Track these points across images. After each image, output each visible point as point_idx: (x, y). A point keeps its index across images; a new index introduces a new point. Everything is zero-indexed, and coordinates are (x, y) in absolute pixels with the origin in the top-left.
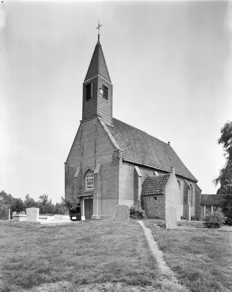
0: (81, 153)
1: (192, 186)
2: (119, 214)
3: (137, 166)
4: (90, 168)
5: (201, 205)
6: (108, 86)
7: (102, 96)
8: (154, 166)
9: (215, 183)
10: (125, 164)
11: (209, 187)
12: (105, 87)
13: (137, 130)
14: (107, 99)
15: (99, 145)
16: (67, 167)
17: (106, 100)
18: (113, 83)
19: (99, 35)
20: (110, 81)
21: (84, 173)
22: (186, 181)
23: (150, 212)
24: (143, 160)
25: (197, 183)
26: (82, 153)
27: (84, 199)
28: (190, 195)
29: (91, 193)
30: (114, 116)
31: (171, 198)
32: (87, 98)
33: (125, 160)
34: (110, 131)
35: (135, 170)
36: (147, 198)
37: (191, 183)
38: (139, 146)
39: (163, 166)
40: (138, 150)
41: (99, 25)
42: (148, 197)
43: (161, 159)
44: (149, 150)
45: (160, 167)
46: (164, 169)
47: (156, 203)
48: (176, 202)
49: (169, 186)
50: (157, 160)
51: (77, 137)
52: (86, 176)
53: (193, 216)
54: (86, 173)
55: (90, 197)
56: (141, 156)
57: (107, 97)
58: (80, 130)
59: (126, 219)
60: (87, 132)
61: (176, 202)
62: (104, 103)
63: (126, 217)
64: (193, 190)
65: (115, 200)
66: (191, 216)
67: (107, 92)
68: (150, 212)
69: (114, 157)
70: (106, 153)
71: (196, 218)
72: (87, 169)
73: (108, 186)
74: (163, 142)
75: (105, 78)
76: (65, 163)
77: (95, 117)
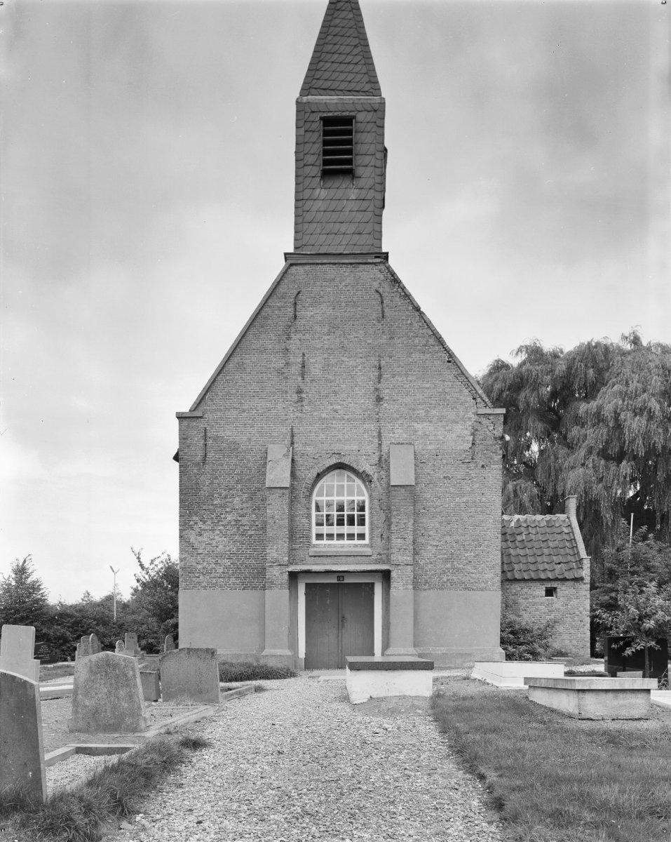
15: (400, 375)
16: (197, 440)
29: (352, 558)
32: (328, 160)
42: (523, 584)
47: (556, 606)
51: (266, 318)
55: (555, 585)
58: (288, 289)
69: (479, 437)
77: (378, 260)
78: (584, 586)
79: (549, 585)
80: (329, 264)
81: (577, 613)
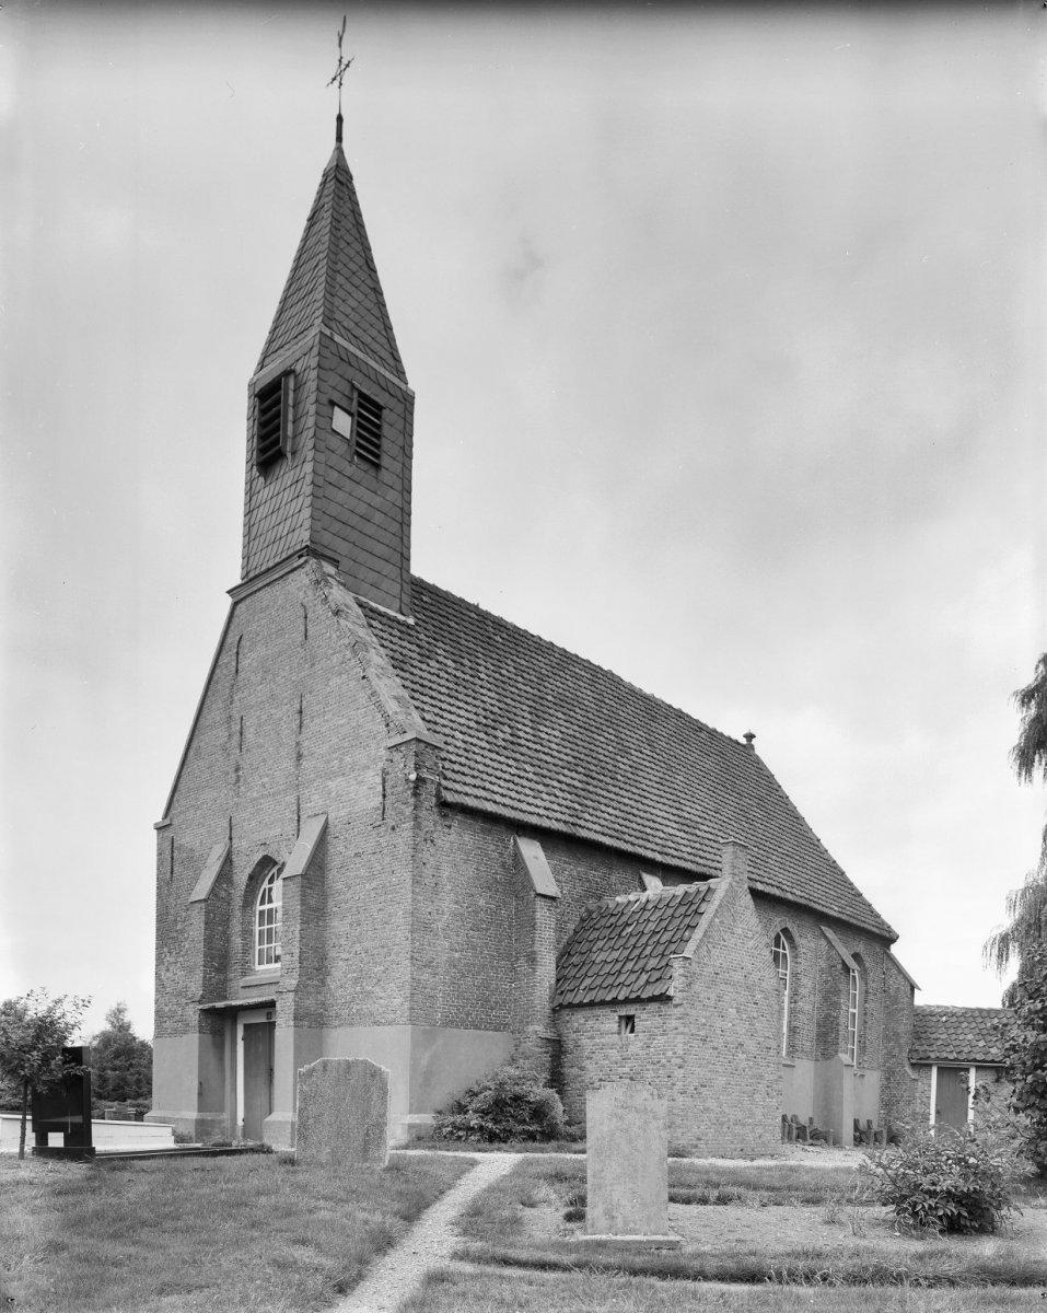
0: (231, 770)
1: (867, 965)
2: (317, 1118)
3: (534, 839)
4: (270, 852)
5: (913, 1065)
6: (381, 399)
7: (343, 448)
8: (641, 842)
9: (994, 958)
11: (957, 964)
12: (362, 395)
13: (567, 660)
14: (377, 467)
17: (372, 472)
18: (415, 382)
19: (340, 119)
20: (401, 373)
21: (241, 878)
22: (829, 933)
24: (577, 806)
26: (237, 770)
28: (856, 1011)
30: (419, 569)
31: (719, 1023)
32: (269, 458)
33: (449, 797)
34: (391, 653)
35: (517, 857)
36: (582, 1021)
37: (860, 947)
38: (561, 736)
39: (697, 845)
40: (555, 753)
41: (340, 61)
44: (625, 761)
45: (675, 853)
46: (701, 861)
48: (751, 1045)
49: (709, 951)
50: (666, 815)
51: (217, 682)
52: (255, 897)
53: (869, 1122)
54: (251, 878)
56: (564, 787)
57: (377, 456)
58: (232, 639)
59: (365, 1150)
60: (261, 651)
62: (360, 491)
63: (366, 1143)
64: (871, 984)
66: (856, 1122)
67: (379, 427)
70: (348, 759)
71: (885, 1135)
72: (257, 857)
73: (358, 947)
74: (713, 733)
75: (364, 346)
76: (159, 829)
77: (302, 560)
78: (675, 1011)
79: (624, 1011)
80: (265, 586)
81: (664, 1061)
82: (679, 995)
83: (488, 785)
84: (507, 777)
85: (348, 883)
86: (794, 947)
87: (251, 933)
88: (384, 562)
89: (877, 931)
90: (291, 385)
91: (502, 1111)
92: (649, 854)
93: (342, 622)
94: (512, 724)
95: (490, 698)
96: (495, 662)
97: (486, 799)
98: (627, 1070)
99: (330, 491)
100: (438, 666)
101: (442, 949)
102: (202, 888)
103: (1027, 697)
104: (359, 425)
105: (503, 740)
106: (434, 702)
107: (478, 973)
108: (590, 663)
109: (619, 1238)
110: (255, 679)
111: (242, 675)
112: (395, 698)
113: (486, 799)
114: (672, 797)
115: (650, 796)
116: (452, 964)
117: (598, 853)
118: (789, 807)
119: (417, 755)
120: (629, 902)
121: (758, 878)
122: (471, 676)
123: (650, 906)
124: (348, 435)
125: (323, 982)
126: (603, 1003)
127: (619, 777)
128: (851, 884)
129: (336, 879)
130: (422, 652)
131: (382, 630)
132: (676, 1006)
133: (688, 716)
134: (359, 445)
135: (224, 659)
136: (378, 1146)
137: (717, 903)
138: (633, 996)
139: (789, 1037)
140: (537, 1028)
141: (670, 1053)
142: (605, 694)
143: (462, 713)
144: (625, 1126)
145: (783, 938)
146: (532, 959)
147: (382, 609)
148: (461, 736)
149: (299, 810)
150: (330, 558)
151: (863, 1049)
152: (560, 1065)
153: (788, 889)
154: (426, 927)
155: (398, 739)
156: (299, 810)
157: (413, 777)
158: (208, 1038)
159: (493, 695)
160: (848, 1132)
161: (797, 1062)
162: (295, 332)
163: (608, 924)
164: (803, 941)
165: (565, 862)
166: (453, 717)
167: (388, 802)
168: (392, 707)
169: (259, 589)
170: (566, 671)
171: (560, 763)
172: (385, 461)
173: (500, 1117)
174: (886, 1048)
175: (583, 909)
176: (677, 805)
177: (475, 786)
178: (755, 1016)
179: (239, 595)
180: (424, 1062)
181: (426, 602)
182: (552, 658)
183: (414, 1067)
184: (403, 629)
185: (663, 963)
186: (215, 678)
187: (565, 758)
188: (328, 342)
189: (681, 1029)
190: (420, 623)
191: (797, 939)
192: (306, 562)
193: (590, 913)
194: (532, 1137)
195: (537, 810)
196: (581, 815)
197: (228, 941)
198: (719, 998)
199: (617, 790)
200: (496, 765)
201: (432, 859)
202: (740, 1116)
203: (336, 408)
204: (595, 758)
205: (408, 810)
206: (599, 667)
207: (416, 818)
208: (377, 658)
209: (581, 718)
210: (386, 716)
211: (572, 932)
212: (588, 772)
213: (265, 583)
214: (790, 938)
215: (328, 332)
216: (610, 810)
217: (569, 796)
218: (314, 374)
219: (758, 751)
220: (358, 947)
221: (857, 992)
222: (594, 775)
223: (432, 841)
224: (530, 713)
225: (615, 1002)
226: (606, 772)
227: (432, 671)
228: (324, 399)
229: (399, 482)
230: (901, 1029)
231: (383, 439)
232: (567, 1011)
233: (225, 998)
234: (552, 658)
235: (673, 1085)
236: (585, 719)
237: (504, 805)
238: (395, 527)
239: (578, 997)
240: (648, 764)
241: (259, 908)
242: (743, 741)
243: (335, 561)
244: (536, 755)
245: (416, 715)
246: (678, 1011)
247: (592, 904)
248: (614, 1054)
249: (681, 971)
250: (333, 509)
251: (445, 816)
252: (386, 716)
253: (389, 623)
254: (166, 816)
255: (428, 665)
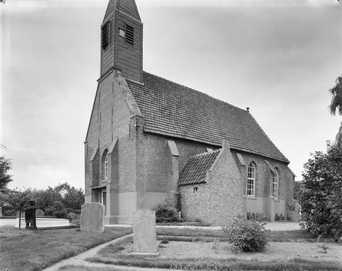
0: (99, 127)
1: (280, 170)
2: (86, 219)
8: (206, 139)
10: (149, 137)
12: (127, 25)
13: (191, 91)
14: (132, 44)
17: (131, 45)
20: (139, 19)
21: (101, 154)
22: (267, 162)
23: (190, 210)
24: (187, 131)
25: (288, 165)
26: (100, 127)
27: (103, 192)
28: (277, 183)
31: (221, 189)
33: (146, 130)
35: (167, 145)
36: (185, 189)
37: (278, 165)
43: (224, 130)
44: (205, 117)
47: (197, 196)
48: (232, 195)
52: (105, 159)
53: (281, 214)
54: (103, 154)
57: (132, 41)
58: (98, 93)
59: (98, 227)
60: (104, 95)
61: (232, 195)
62: (128, 51)
63: (98, 225)
65: (133, 193)
67: (133, 33)
68: (190, 210)
69: (131, 128)
71: (286, 218)
72: (104, 149)
73: (125, 172)
74: (236, 109)
76: (85, 143)
77: (112, 70)
82: (208, 181)
83: (159, 127)
84: (166, 124)
85: (122, 154)
86: (256, 166)
87: (104, 169)
88: (135, 69)
89: (283, 161)
90: (109, 25)
91: (160, 214)
92: (208, 143)
93: (121, 86)
94: (170, 110)
95: (164, 103)
96: (168, 93)
97: (158, 130)
98: (196, 202)
99: (119, 52)
100: (149, 95)
101: (145, 171)
102: (92, 158)
103: (333, 91)
104: (127, 33)
105: (167, 114)
106: (146, 105)
107: (157, 177)
108: (199, 92)
109: (142, 254)
110: (103, 103)
111: (101, 102)
112: (133, 105)
113: (158, 130)
114: (219, 126)
115: (212, 127)
116: (149, 175)
117: (193, 143)
118: (259, 127)
119: (137, 120)
120: (200, 156)
121: (244, 148)
122: (159, 97)
123: (204, 157)
124: (124, 37)
125: (118, 181)
126: (189, 184)
127: (202, 122)
128: (276, 148)
129: (120, 154)
130: (145, 92)
131: (133, 87)
132: (207, 184)
133: (228, 104)
134: (127, 39)
135: (97, 98)
136: (101, 226)
137: (220, 155)
138: (197, 182)
139: (255, 191)
140: (173, 191)
141: (206, 198)
142: (202, 100)
143: (155, 107)
144: (143, 222)
145: (253, 164)
146: (172, 173)
147: (134, 82)
148: (153, 114)
149: (112, 136)
150: (120, 69)
151: (279, 194)
152: (180, 201)
153: (253, 150)
154: (141, 166)
155: (132, 116)
156: (112, 136)
157: (135, 125)
158: (94, 196)
159: (165, 102)
160: (273, 217)
161: (258, 198)
162: (110, 12)
163: (194, 162)
164: (259, 164)
165: (183, 146)
166: (152, 109)
167: (131, 133)
168: (131, 107)
169: (104, 79)
170: (190, 94)
171: (183, 119)
172: (135, 42)
173: (160, 216)
174: (286, 193)
175: (189, 159)
176: (220, 129)
177: (155, 127)
178: (233, 186)
179: (100, 81)
180: (141, 201)
181: (149, 79)
182: (186, 91)
183: (138, 203)
184: (140, 86)
185: (205, 173)
186: (95, 103)
187: (186, 118)
188: (117, 13)
189: (209, 191)
190: (146, 84)
191: (257, 164)
192: (113, 71)
193: (190, 159)
194: (169, 221)
195: (173, 132)
196: (187, 133)
197: (99, 171)
198: (221, 182)
199: (201, 126)
200: (163, 121)
201: (142, 147)
202: (229, 214)
203: (120, 30)
204: (195, 117)
205: (135, 135)
206: (201, 92)
207: (137, 136)
208: (129, 94)
209: (193, 107)
210: (130, 110)
211: (185, 165)
212: (192, 121)
213: (105, 77)
214: (255, 164)
215: (117, 10)
216: (198, 131)
217: (185, 128)
218: (114, 21)
219: (250, 112)
220: (125, 172)
221: (277, 178)
222: (194, 122)
223: (142, 142)
224: (176, 106)
225: (192, 184)
226: (198, 121)
227: (147, 97)
228: (117, 28)
229: (139, 47)
230: (291, 188)
231: (134, 37)
232: (182, 187)
233: (98, 186)
234: (186, 91)
235: (207, 206)
236: (194, 107)
237: (163, 132)
238: (138, 60)
239: (184, 183)
240: (212, 118)
241: (106, 162)
242: (246, 110)
243: (120, 70)
244: (176, 117)
245: (138, 109)
246: (208, 186)
247: (191, 157)
248: (193, 198)
249: (208, 175)
250: (120, 56)
251: (146, 136)
252: (130, 110)
253: (136, 85)
254: (86, 140)
255: (146, 95)
